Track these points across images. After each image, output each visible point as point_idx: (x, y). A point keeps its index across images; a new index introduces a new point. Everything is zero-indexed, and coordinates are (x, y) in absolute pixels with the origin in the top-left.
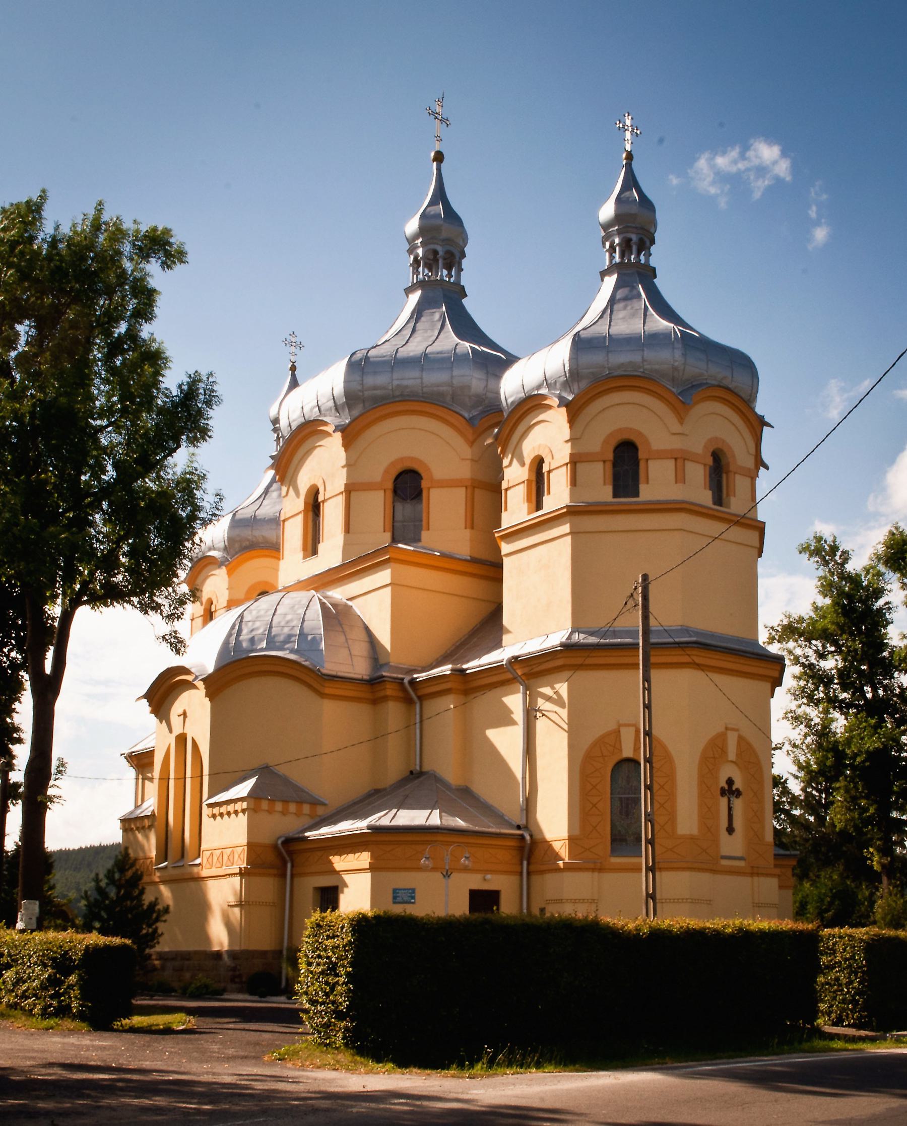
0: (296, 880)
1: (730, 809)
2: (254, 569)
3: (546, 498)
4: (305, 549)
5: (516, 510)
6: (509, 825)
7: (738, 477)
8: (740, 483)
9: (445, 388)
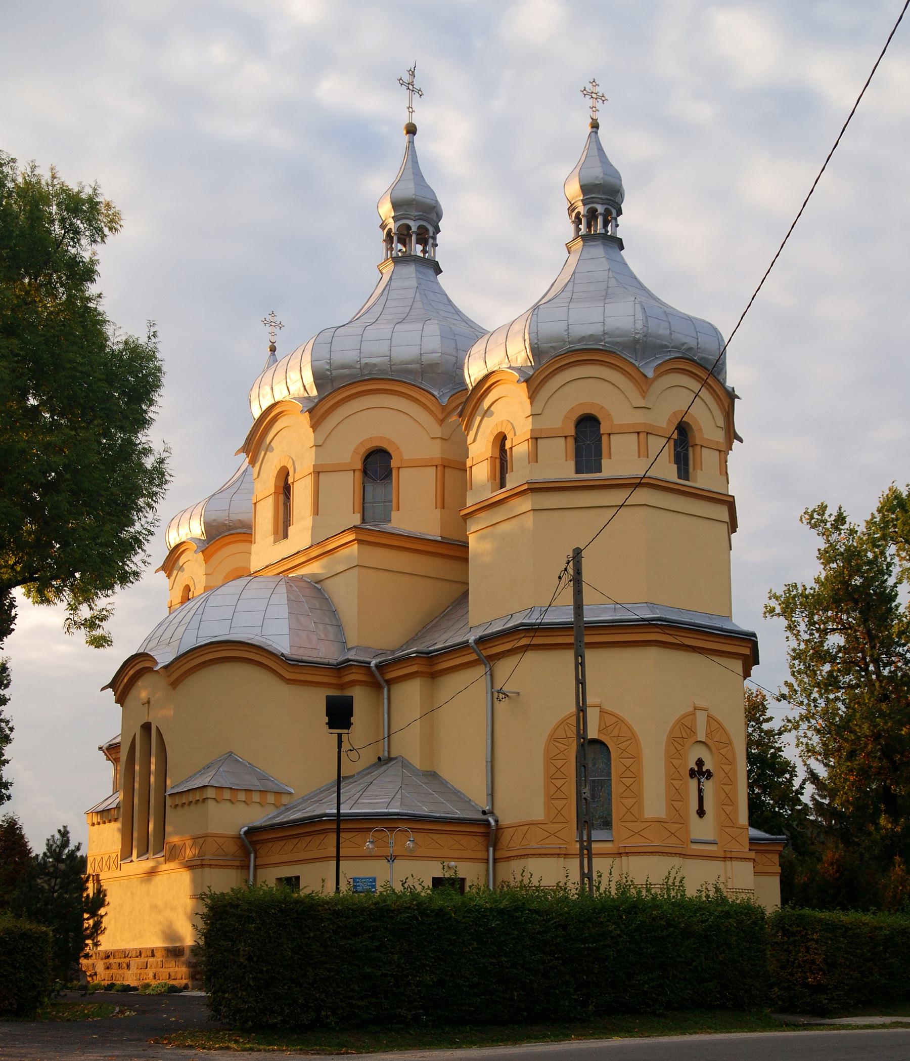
0: (259, 871)
1: (700, 791)
2: (228, 556)
4: (276, 532)
8: (709, 458)
9: (414, 366)
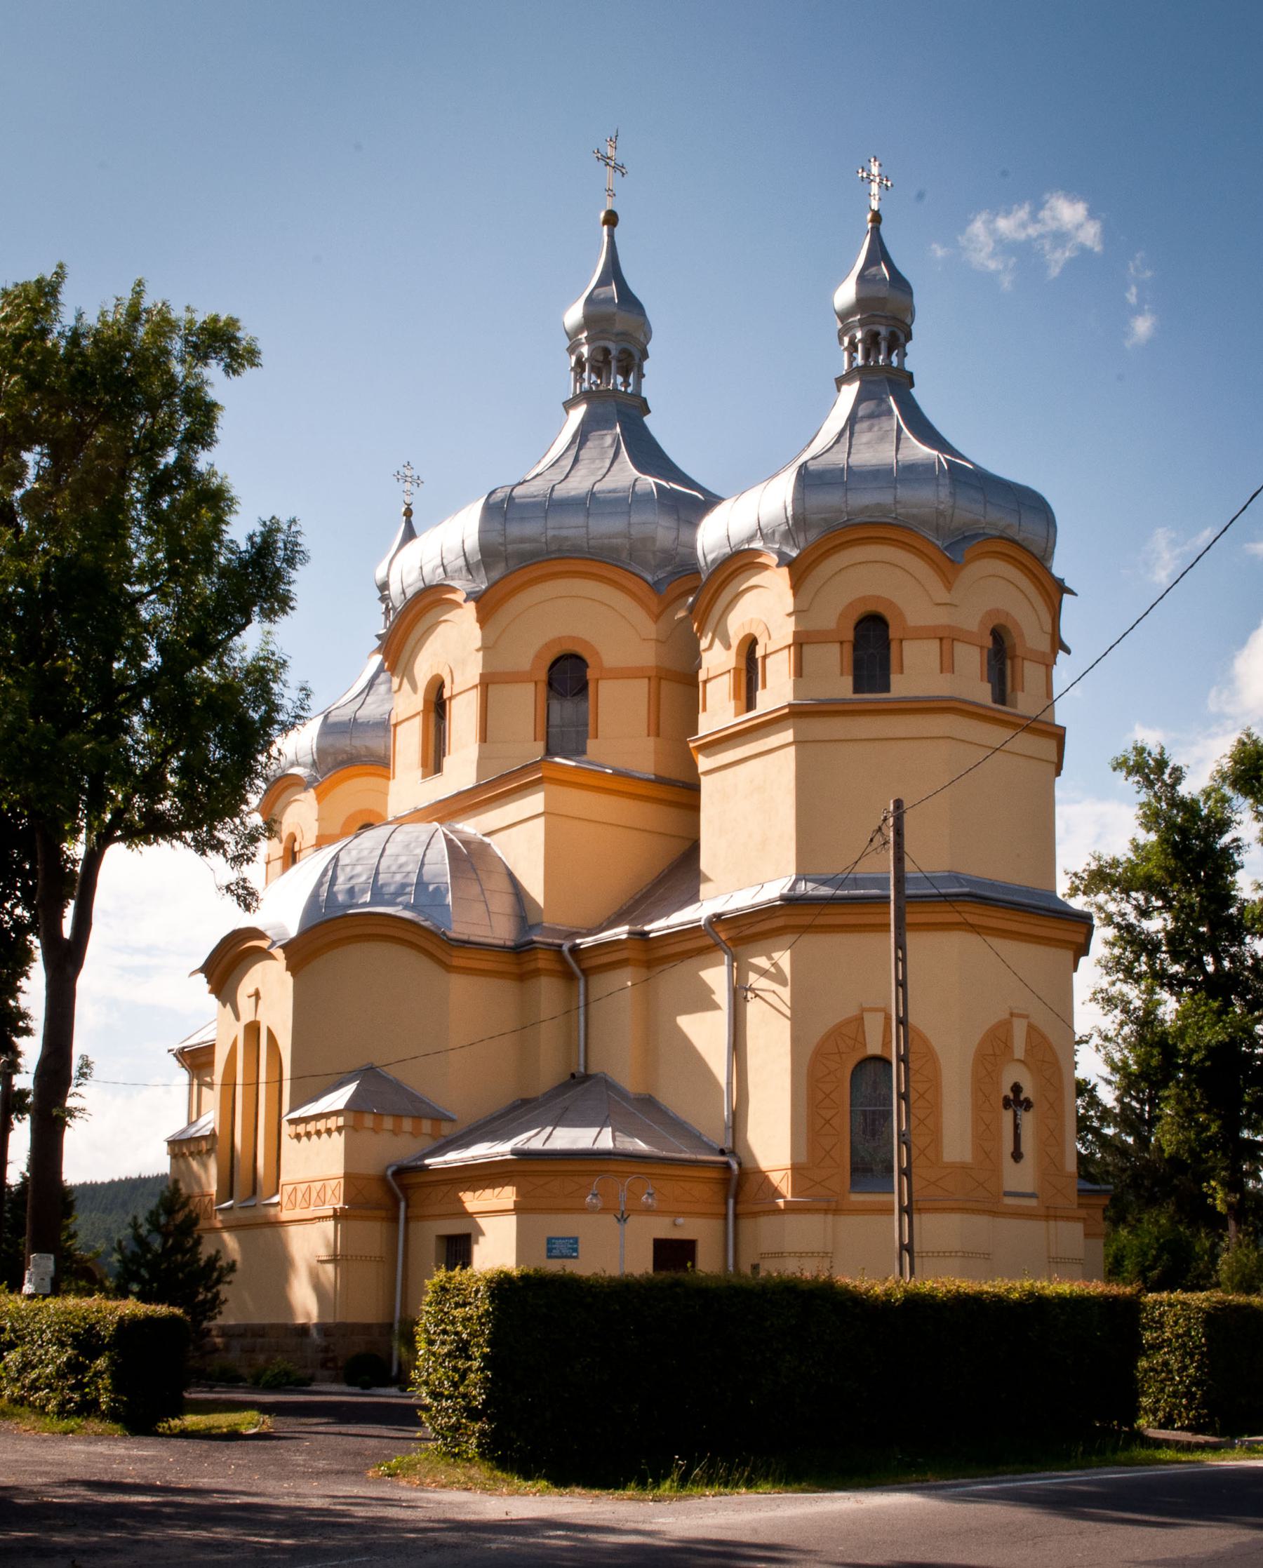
0: (412, 1225)
1: (1016, 1126)
2: (354, 792)
3: (761, 695)
4: (424, 764)
5: (718, 711)
6: (710, 1148)
7: (1027, 663)
8: (1031, 672)
